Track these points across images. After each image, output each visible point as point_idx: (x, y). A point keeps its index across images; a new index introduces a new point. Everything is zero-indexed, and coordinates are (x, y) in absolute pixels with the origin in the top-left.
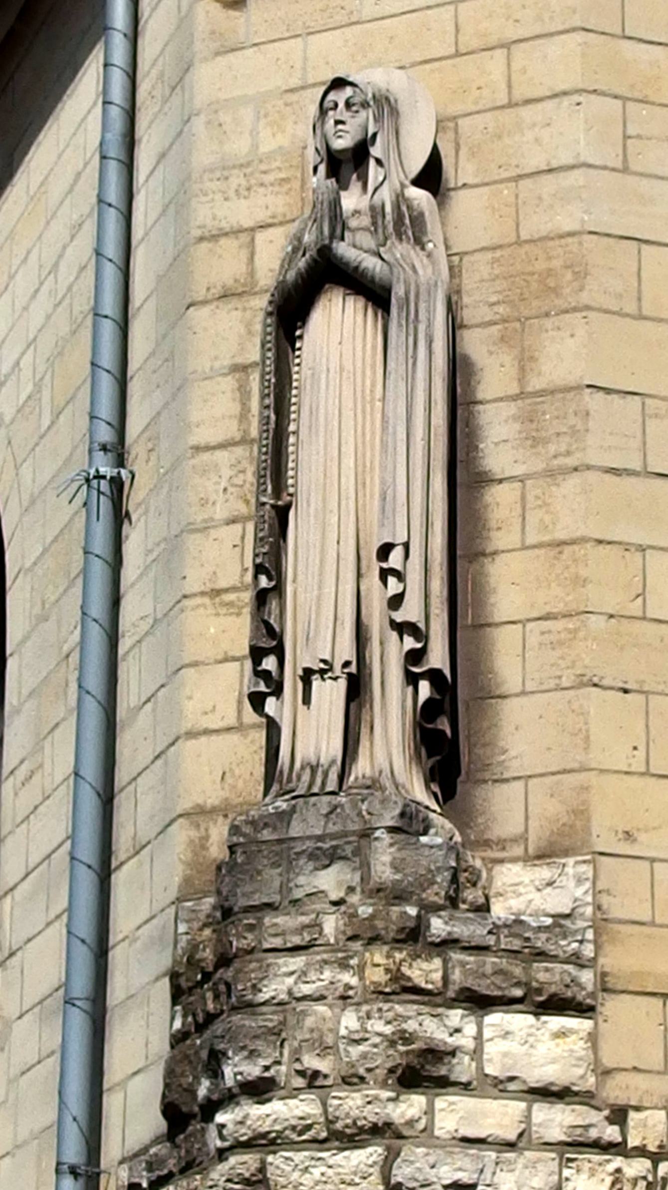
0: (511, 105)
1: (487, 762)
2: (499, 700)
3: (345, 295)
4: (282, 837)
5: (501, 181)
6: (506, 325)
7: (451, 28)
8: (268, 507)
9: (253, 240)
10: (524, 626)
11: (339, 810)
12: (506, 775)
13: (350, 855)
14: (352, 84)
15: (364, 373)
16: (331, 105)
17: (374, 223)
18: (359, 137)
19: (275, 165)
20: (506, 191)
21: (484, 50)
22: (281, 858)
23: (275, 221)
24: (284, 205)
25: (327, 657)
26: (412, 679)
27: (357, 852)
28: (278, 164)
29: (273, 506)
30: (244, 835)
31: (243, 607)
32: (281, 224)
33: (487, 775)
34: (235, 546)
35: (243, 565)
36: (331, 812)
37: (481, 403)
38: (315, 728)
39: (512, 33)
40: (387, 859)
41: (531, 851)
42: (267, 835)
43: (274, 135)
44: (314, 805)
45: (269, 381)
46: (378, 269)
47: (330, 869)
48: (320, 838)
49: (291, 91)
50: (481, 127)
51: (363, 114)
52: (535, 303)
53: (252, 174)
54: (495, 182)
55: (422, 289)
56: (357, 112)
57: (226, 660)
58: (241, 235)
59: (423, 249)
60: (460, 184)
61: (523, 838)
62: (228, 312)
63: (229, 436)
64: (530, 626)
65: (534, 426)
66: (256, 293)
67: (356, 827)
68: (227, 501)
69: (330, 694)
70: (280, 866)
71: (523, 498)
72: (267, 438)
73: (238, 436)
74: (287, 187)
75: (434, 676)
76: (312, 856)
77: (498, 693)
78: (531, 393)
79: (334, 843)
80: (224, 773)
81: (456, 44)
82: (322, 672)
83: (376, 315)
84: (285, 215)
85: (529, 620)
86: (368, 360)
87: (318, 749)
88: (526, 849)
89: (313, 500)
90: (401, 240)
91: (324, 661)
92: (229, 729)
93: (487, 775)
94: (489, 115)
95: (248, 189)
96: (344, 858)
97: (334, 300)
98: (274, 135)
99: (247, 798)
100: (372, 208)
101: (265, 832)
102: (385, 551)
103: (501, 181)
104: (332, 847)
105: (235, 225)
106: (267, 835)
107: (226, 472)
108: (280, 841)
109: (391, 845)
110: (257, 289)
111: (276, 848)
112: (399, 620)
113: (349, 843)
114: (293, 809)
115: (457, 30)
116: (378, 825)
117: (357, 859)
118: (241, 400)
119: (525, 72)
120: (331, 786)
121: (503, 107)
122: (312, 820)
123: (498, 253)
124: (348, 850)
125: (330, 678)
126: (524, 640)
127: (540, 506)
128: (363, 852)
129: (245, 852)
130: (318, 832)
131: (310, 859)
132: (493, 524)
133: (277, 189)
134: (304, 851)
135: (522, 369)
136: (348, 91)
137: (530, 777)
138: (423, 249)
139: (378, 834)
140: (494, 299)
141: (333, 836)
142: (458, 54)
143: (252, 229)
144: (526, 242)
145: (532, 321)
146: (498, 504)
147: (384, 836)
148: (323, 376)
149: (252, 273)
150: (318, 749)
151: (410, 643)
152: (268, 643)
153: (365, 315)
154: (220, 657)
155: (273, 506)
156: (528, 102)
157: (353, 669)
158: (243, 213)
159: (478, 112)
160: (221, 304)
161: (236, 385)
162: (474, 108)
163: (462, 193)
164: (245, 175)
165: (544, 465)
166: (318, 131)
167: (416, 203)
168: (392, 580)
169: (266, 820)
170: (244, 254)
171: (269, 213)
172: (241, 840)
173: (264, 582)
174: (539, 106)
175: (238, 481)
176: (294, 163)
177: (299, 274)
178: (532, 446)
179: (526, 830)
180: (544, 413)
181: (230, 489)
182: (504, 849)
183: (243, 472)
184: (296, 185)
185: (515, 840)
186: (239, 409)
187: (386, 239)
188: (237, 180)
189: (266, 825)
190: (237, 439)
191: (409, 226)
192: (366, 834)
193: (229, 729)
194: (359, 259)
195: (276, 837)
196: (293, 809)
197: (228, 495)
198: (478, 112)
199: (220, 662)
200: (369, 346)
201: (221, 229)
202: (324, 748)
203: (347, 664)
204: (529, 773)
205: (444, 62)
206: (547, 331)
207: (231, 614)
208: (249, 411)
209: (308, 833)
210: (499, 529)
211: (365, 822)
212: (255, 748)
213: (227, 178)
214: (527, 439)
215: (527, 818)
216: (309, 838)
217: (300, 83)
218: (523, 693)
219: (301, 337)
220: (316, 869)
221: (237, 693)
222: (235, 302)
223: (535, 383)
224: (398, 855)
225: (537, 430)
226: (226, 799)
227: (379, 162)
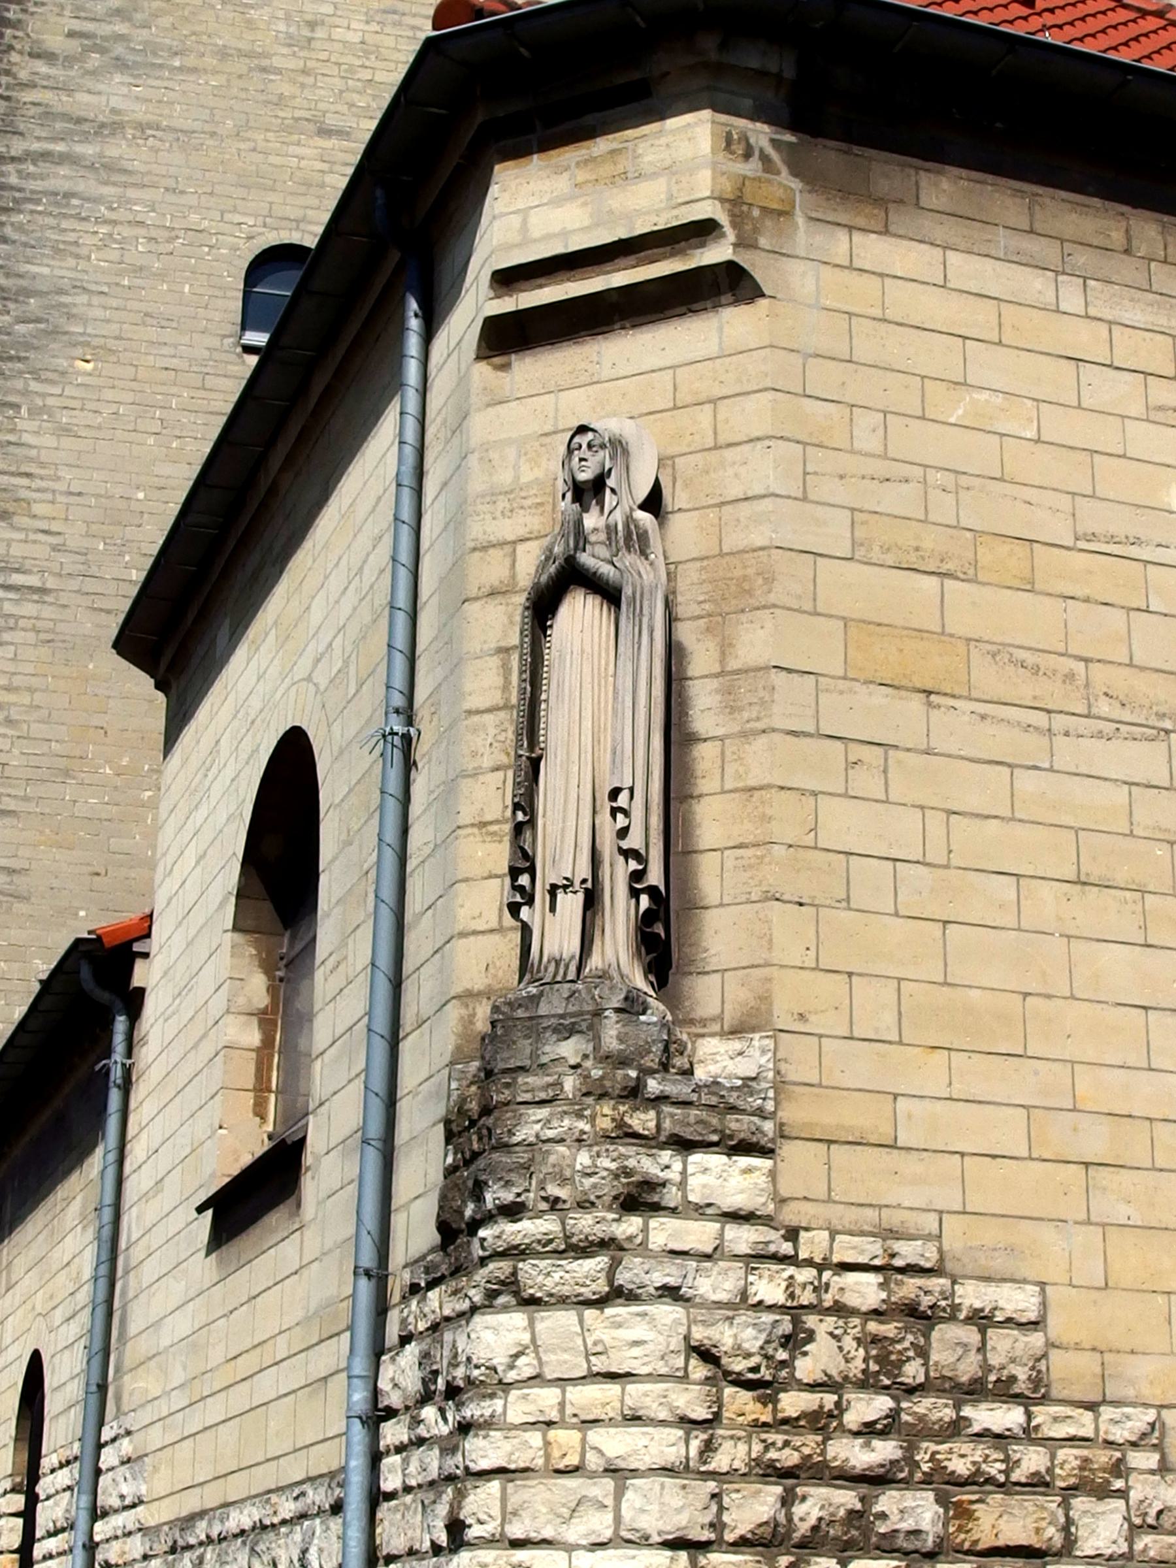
0: (716, 447)
5: (709, 507)
9: (514, 550)
15: (600, 654)
16: (577, 446)
17: (609, 539)
18: (598, 471)
20: (712, 514)
25: (569, 875)
26: (635, 894)
27: (591, 1027)
28: (534, 491)
29: (528, 758)
30: (503, 1013)
32: (537, 538)
33: (692, 969)
36: (571, 996)
37: (691, 679)
39: (718, 392)
40: (614, 1033)
41: (726, 1028)
42: (520, 1013)
46: (611, 574)
47: (569, 1041)
48: (562, 1016)
49: (546, 435)
50: (693, 465)
51: (601, 453)
52: (734, 602)
53: (514, 499)
54: (704, 507)
57: (490, 877)
59: (647, 559)
61: (720, 1018)
63: (495, 702)
64: (727, 853)
65: (732, 697)
67: (590, 1008)
69: (571, 904)
71: (723, 753)
75: (652, 891)
76: (556, 1030)
79: (573, 1020)
82: (565, 887)
86: (603, 645)
87: (561, 947)
88: (722, 1026)
89: (559, 753)
92: (492, 931)
93: (692, 969)
94: (699, 455)
100: (608, 527)
102: (614, 793)
103: (709, 507)
106: (520, 1013)
107: (492, 731)
108: (531, 1018)
109: (617, 1022)
113: (584, 1020)
114: (541, 994)
115: (675, 389)
120: (571, 975)
122: (556, 1003)
123: (705, 563)
124: (584, 1026)
130: (561, 1012)
132: (699, 773)
133: (533, 511)
135: (723, 653)
136: (590, 435)
138: (647, 559)
139: (607, 1013)
141: (572, 1015)
144: (727, 554)
148: (568, 657)
149: (513, 576)
150: (561, 947)
151: (633, 865)
152: (523, 864)
154: (485, 875)
155: (528, 758)
156: (730, 445)
159: (690, 453)
167: (641, 523)
168: (620, 816)
170: (507, 562)
173: (520, 816)
174: (739, 449)
176: (548, 491)
177: (551, 577)
179: (723, 1012)
180: (740, 688)
181: (495, 744)
182: (705, 1026)
183: (505, 731)
185: (713, 1019)
187: (618, 551)
188: (503, 503)
189: (520, 1006)
191: (636, 541)
192: (598, 1013)
193: (492, 931)
195: (528, 1015)
196: (541, 994)
198: (690, 453)
200: (604, 634)
202: (566, 947)
203: (584, 881)
210: (704, 777)
215: (723, 1002)
216: (553, 1016)
217: (552, 429)
218: (721, 905)
219: (551, 626)
220: (559, 1040)
222: (499, 599)
224: (622, 1030)
227: (613, 491)
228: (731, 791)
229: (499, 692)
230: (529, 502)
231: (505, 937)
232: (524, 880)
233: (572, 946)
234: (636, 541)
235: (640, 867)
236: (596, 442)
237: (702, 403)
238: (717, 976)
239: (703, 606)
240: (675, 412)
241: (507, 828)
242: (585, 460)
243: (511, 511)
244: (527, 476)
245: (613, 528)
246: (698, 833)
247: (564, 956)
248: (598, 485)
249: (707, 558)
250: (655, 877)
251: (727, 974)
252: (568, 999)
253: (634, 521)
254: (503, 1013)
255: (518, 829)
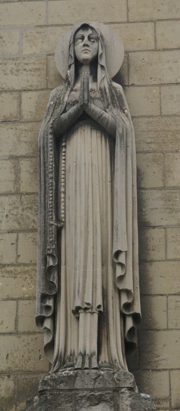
0: (156, 50)
1: (150, 361)
2: (155, 331)
3: (91, 129)
4: (71, 388)
5: (152, 86)
6: (156, 154)
7: (125, 8)
8: (54, 227)
9: (20, 96)
10: (167, 297)
11: (101, 377)
12: (160, 368)
13: (109, 400)
14: (92, 28)
15: (102, 169)
16: (80, 37)
17: (102, 96)
18: (95, 54)
19: (31, 61)
20: (155, 91)
21: (141, 22)
22: (72, 398)
23: (32, 88)
24: (37, 82)
25: (90, 302)
26: (123, 317)
27: (112, 398)
28: (33, 61)
29: (56, 226)
30: (50, 386)
31: (18, 274)
32: (36, 90)
33: (149, 367)
34: (12, 244)
35: (17, 254)
36: (97, 378)
37: (144, 189)
38: (81, 337)
39: (156, 16)
40: (128, 403)
41: (173, 405)
42: (62, 386)
43: (31, 46)
44: (88, 374)
45: (52, 165)
46: (110, 119)
47: (98, 406)
48: (92, 390)
49: (41, 26)
50: (141, 58)
51: (96, 44)
52: (170, 146)
53: (19, 64)
54: (148, 86)
55: (129, 131)
56: (94, 42)
57: (8, 299)
58: (13, 93)
59: (124, 112)
60: (130, 84)
61: (169, 399)
62: (7, 129)
63: (9, 190)
64: (170, 297)
65: (171, 203)
66: (22, 122)
67: (112, 386)
68: (8, 221)
69: (89, 322)
70: (71, 402)
71: (166, 236)
72: (52, 193)
73: (13, 191)
74: (38, 73)
75: (135, 317)
76: (89, 399)
77: (154, 328)
78: (169, 187)
79: (100, 393)
80: (8, 355)
81: (128, 16)
82: (86, 309)
83: (106, 141)
84: (37, 86)
85: (169, 295)
86: (104, 162)
87: (85, 347)
88: (171, 404)
89: (78, 225)
90: (114, 107)
91: (88, 304)
92: (10, 334)
93: (149, 367)
94: (145, 53)
95: (18, 71)
96: (106, 401)
97: (86, 131)
98: (31, 46)
99: (21, 368)
100: (101, 89)
101: (62, 385)
102: (118, 253)
103: (152, 86)
104: (100, 395)
105: (11, 88)
106: (62, 386)
107: (7, 208)
108: (70, 390)
109: (130, 396)
110: (23, 120)
111: (69, 393)
112: (120, 288)
113: (109, 393)
114: (76, 375)
115: (128, 10)
116: (124, 386)
117: (112, 402)
118: (15, 173)
119: (163, 36)
120: (95, 365)
121: (152, 50)
122: (87, 381)
123: (151, 119)
124: (108, 397)
125: (90, 312)
126: (167, 304)
127: (174, 242)
128: (115, 398)
129: (52, 394)
130: (91, 387)
131: (88, 400)
132: (151, 247)
133: (33, 73)
134: (85, 396)
135: (164, 175)
136: (90, 32)
137: (172, 369)
138: (124, 112)
139: (123, 390)
140: (149, 140)
141: (99, 390)
142: (128, 22)
143: (20, 91)
144: (165, 116)
145: (169, 154)
146: (153, 238)
147: (127, 391)
148: (83, 167)
149: (20, 112)
150: (85, 347)
151: (125, 299)
152: (51, 292)
153: (101, 140)
154: (5, 297)
155: (56, 226)
156: (164, 50)
157: (102, 309)
158: (15, 82)
159: (139, 51)
160: (3, 125)
161: (12, 166)
162: (137, 49)
163: (131, 88)
164: (15, 64)
165: (176, 222)
166: (72, 48)
167: (118, 89)
168: (119, 269)
169: (62, 379)
170: (16, 102)
171: (29, 84)
172: (49, 388)
173: (51, 262)
174: (171, 53)
175: (15, 212)
176: (43, 62)
177: (70, 116)
178: (170, 212)
179: (170, 395)
180: (176, 197)
181: (10, 216)
182: (159, 403)
183: (17, 208)
184: (43, 72)
185: (165, 399)
186: (14, 177)
187: (108, 105)
188: (11, 65)
189: (62, 382)
190: (13, 192)
191: (116, 101)
192: (117, 390)
193: (10, 334)
194: (101, 113)
195: (68, 388)
196: (76, 375)
197: (8, 219)
198: (139, 51)
199: (5, 300)
200: (104, 155)
201: (3, 88)
202: (88, 346)
203: (99, 307)
204: (171, 368)
205: (121, 25)
206: (177, 159)
207: (11, 277)
208: (20, 179)
209: (86, 387)
210: (153, 250)
211: (116, 384)
212: (25, 344)
213: (5, 64)
214: (167, 208)
215: (170, 389)
216: (86, 389)
217: (45, 23)
218: (167, 329)
219: (65, 146)
220: (91, 405)
221: (15, 316)
222: (10, 125)
223: (171, 183)
224: (133, 402)
225: (172, 205)
226: (9, 368)
227: (102, 67)
228: (172, 260)
229: (12, 183)
230: (28, 67)
231: (20, 337)
232: (50, 303)
233: (92, 346)
234: (116, 101)
235: (130, 301)
236: (94, 36)
237: (148, 22)
238: (166, 373)
239: (150, 145)
240: (128, 24)
241: (39, 268)
242: (87, 46)
243: (18, 71)
244: (27, 52)
245: (103, 91)
246: (151, 284)
247: (88, 352)
248: (94, 63)
249: (152, 116)
250: (137, 309)
251: (172, 372)
252: (95, 380)
253: (114, 87)
254: (50, 386)
255: (48, 271)
